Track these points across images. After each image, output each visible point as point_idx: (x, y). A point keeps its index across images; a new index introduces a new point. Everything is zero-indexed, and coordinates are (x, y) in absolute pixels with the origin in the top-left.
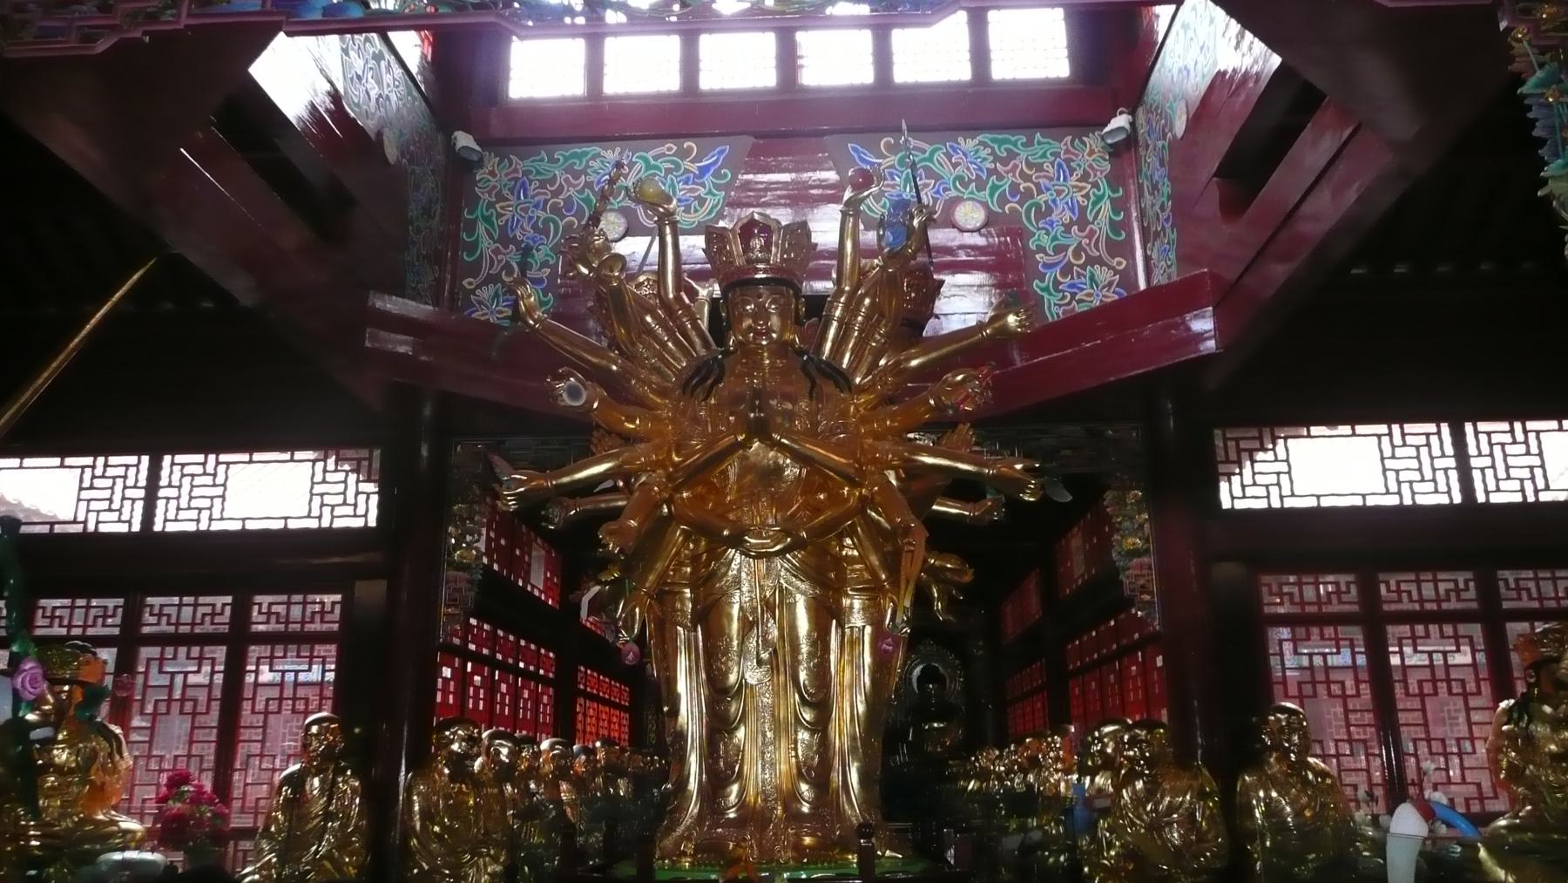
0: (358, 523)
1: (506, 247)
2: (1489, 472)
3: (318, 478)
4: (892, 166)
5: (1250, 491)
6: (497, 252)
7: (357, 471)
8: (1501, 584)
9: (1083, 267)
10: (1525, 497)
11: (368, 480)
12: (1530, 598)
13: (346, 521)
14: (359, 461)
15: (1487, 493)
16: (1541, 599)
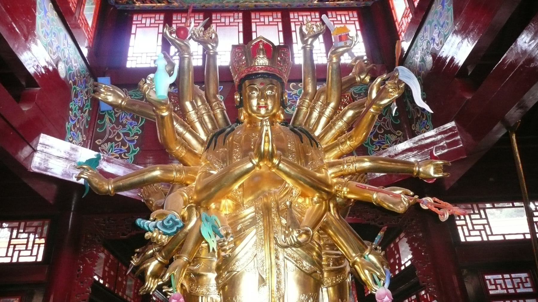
0: (32, 259)
1: (118, 126)
2: (465, 227)
3: (14, 235)
4: (296, 94)
5: (472, 233)
6: (113, 128)
7: (35, 233)
8: (488, 282)
9: (382, 134)
10: (482, 238)
11: (40, 238)
12: (502, 289)
13: (26, 258)
14: (37, 227)
15: (465, 237)
16: (507, 289)
